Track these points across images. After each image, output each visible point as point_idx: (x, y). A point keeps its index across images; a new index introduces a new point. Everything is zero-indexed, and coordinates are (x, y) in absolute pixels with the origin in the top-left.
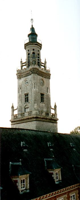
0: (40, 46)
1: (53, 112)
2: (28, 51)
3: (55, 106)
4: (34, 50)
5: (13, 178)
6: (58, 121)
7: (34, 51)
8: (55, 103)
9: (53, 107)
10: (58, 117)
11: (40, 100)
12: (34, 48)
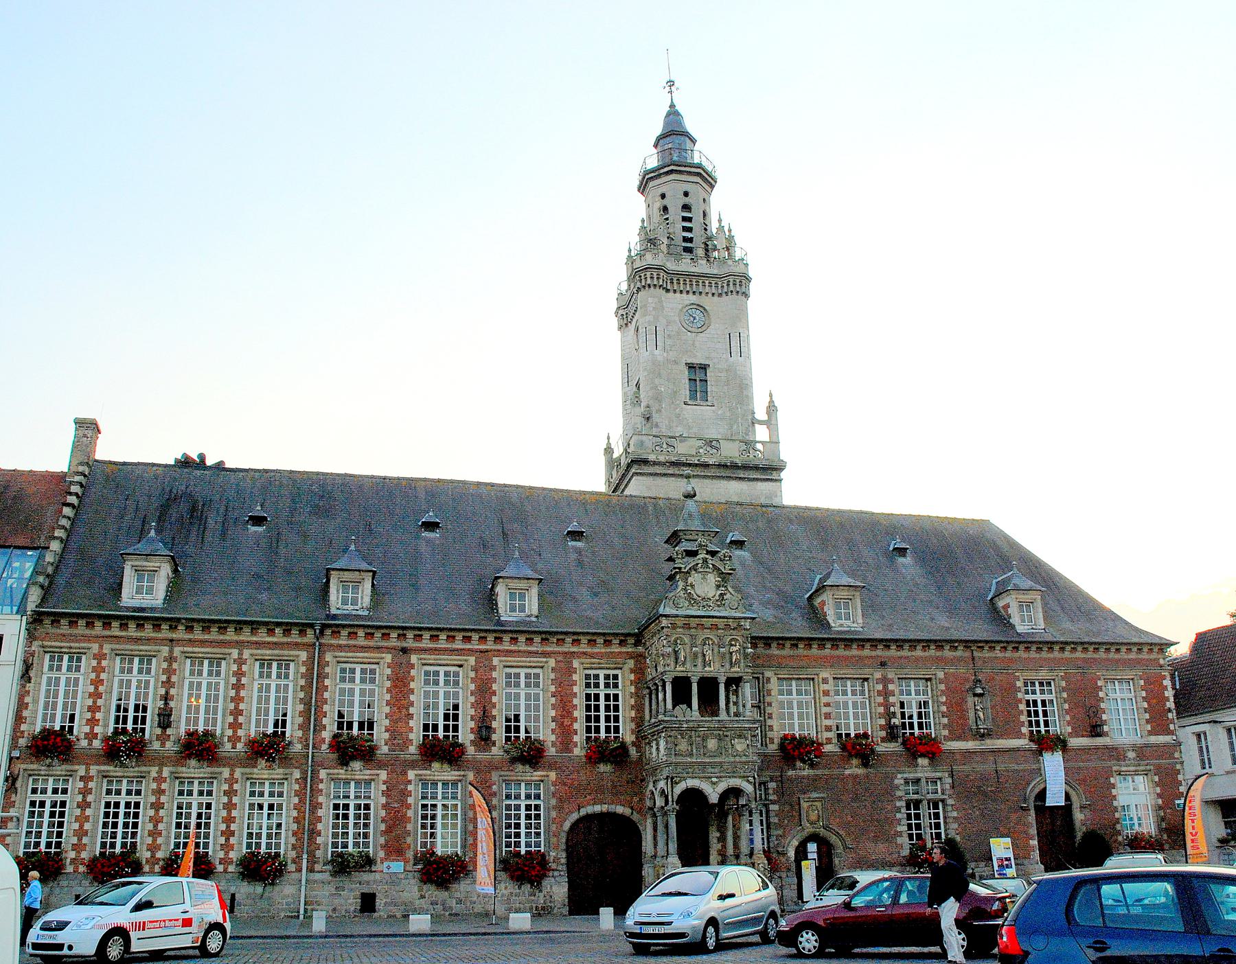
0: (707, 179)
1: (762, 433)
2: (663, 196)
3: (772, 409)
4: (695, 666)
5: (25, 574)
6: (783, 475)
7: (686, 200)
8: (771, 395)
9: (761, 414)
10: (785, 453)
11: (685, 392)
12: (688, 190)
